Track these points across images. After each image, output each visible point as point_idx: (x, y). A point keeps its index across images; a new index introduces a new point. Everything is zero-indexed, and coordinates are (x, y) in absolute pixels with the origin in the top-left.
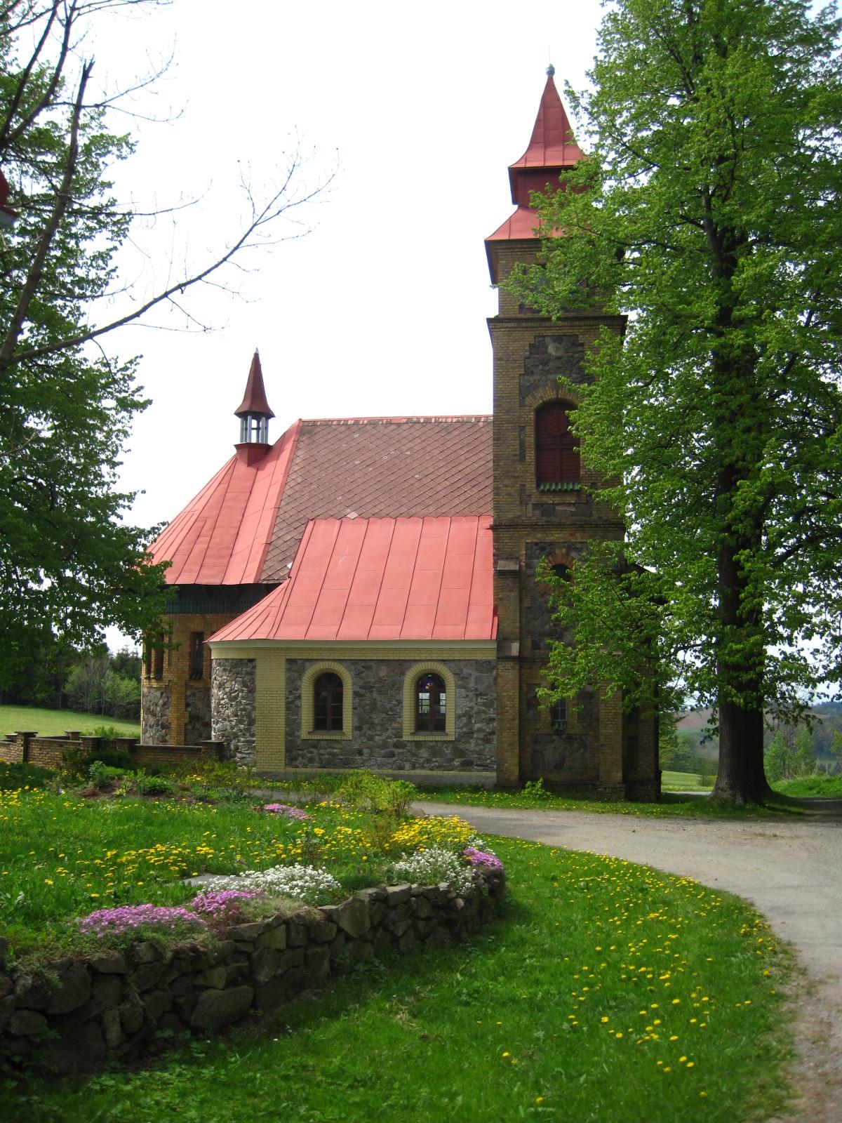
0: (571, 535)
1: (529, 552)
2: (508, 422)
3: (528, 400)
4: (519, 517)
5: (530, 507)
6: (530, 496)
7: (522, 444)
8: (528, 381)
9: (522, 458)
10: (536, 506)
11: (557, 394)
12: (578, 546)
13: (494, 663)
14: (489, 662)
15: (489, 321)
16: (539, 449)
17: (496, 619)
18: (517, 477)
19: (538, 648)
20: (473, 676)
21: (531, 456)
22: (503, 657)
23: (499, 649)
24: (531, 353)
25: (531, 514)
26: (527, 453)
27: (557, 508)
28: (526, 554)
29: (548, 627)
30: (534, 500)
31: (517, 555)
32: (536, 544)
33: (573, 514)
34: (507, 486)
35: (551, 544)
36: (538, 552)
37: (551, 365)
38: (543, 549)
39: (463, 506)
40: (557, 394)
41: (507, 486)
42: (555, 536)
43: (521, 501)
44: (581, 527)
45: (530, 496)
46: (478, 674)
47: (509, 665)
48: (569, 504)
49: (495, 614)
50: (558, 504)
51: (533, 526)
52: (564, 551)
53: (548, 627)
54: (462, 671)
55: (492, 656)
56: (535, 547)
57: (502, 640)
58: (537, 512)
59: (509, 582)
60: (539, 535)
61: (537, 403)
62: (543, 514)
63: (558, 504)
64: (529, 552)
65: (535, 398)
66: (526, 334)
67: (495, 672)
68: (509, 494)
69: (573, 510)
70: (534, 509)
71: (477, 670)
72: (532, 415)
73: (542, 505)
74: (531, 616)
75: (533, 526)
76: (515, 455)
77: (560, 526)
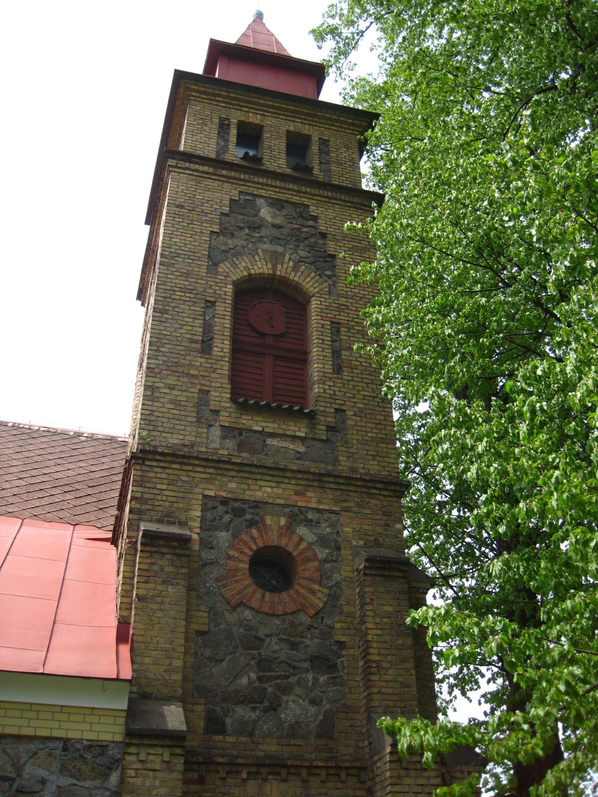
0: (297, 493)
1: (209, 515)
2: (183, 290)
3: (223, 267)
4: (193, 445)
5: (216, 432)
6: (216, 412)
7: (208, 328)
8: (225, 244)
9: (206, 346)
10: (228, 431)
11: (274, 268)
12: (310, 516)
13: (113, 752)
14: (100, 748)
15: (180, 77)
16: (238, 349)
17: (125, 649)
18: (193, 376)
19: (222, 731)
20: (51, 788)
21: (222, 346)
22: (141, 732)
23: (131, 713)
24: (231, 211)
25: (214, 442)
26: (217, 343)
27: (269, 441)
28: (203, 519)
29: (244, 681)
30: (225, 419)
31: (183, 518)
32: (225, 502)
33: (300, 456)
34: (172, 388)
35: (257, 505)
36: (227, 518)
37: (264, 232)
38: (238, 513)
39: (47, 509)
40: (274, 268)
41: (172, 388)
42: (265, 491)
43: (199, 420)
44: (319, 480)
45: (216, 412)
46: (66, 781)
47: (156, 757)
48: (294, 438)
49: (122, 636)
50: (273, 435)
51: (219, 465)
52: (283, 521)
53: (244, 681)
54: (19, 769)
55: (110, 731)
56: (221, 509)
57: (141, 695)
58: (230, 444)
59: (165, 563)
60: (232, 485)
61: (239, 274)
62: (241, 447)
63: (273, 435)
64: (209, 515)
65: (235, 266)
66: (226, 186)
67: (114, 778)
68: (176, 403)
69: (302, 449)
70: (223, 438)
71: (64, 770)
72: (229, 289)
73: (241, 431)
74: (208, 652)
75: (219, 465)
76: (192, 341)
77: (277, 472)
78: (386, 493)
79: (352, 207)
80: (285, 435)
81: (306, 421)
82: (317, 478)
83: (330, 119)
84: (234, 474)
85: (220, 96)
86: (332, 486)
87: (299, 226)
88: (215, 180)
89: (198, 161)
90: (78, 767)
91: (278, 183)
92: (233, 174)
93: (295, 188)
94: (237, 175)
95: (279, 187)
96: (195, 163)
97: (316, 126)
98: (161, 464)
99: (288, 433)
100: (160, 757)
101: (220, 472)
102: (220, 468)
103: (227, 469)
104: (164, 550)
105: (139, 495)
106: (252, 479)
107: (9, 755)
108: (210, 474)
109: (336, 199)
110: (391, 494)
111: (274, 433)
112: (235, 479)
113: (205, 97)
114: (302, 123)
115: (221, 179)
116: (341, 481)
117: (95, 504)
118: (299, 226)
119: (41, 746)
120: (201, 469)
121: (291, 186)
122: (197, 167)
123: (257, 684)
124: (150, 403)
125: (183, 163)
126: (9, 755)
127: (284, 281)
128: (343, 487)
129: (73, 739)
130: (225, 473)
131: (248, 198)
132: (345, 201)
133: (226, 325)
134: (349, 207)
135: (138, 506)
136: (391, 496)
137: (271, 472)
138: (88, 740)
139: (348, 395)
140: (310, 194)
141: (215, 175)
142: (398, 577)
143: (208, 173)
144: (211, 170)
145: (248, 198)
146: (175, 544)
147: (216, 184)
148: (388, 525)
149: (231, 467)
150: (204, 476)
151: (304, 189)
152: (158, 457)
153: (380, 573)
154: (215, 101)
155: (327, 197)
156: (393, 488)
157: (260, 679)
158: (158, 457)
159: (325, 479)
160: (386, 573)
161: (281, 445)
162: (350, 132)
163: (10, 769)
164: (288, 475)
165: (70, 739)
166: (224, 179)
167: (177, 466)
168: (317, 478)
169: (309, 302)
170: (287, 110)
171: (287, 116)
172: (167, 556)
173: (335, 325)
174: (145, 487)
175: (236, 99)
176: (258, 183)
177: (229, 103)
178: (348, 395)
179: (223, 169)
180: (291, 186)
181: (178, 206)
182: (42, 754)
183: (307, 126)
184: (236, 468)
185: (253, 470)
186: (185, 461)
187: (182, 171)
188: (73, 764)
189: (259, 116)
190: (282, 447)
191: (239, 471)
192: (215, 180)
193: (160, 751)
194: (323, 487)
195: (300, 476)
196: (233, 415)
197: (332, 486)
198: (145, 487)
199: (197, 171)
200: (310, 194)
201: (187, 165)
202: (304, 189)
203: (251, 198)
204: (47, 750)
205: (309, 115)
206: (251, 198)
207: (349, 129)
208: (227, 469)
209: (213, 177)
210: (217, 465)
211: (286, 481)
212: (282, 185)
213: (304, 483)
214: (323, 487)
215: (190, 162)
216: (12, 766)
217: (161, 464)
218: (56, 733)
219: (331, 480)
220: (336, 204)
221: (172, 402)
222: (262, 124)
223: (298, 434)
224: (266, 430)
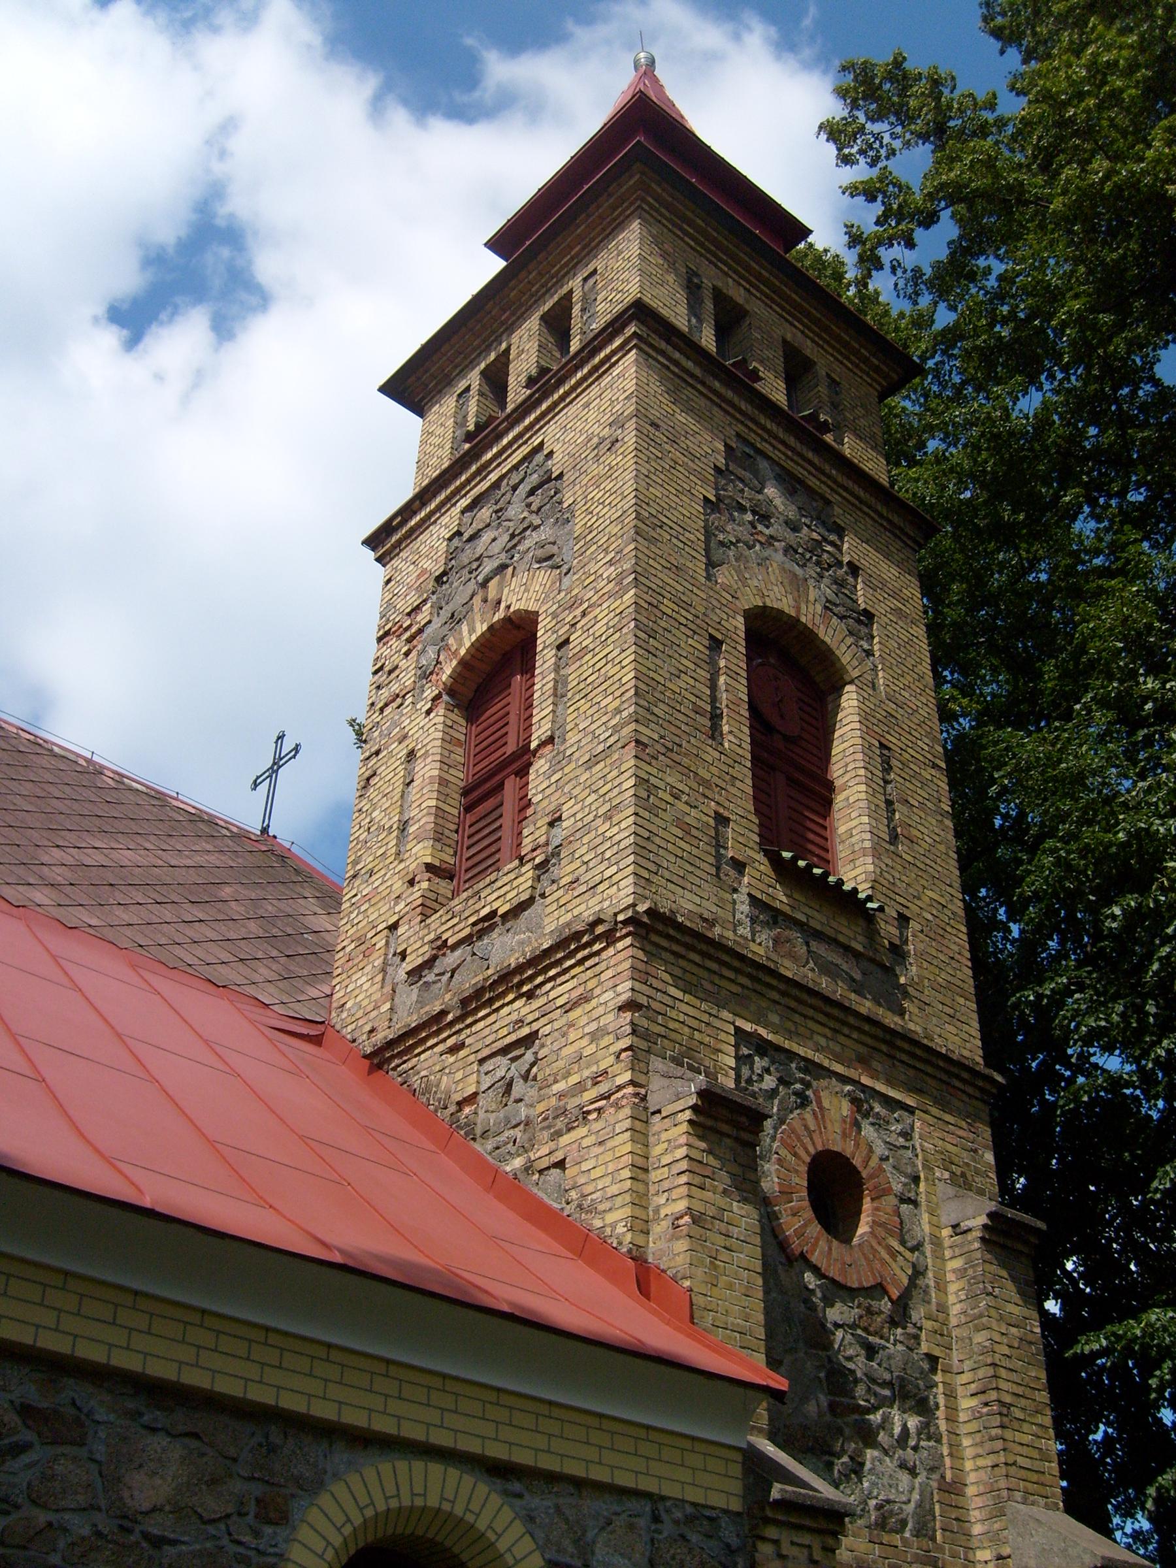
21: (736, 734)
78: (970, 1090)
79: (890, 531)
80: (835, 941)
81: (861, 922)
82: (888, 1037)
83: (846, 345)
84: (775, 996)
85: (690, 223)
86: (905, 1058)
87: (819, 538)
88: (701, 393)
89: (682, 345)
90: (678, 1557)
91: (792, 441)
92: (730, 394)
93: (816, 460)
94: (736, 400)
95: (793, 450)
96: (676, 347)
97: (822, 348)
98: (675, 948)
99: (841, 938)
100: (805, 1551)
101: (758, 987)
102: (758, 980)
103: (769, 986)
104: (725, 1128)
105: (643, 1000)
106: (801, 1015)
107: (567, 1521)
108: (742, 986)
109: (870, 507)
110: (978, 1094)
111: (822, 933)
112: (778, 1007)
113: (667, 214)
114: (803, 332)
115: (711, 395)
116: (919, 1052)
117: (13, 868)
118: (819, 538)
119: (618, 1509)
120: (732, 975)
121: (810, 455)
122: (677, 355)
123: (828, 1418)
124: (646, 815)
125: (657, 338)
126: (567, 1521)
127: (807, 637)
128: (918, 1065)
129: (670, 1498)
130: (764, 990)
131: (747, 450)
132: (881, 515)
133: (741, 695)
134: (885, 528)
135: (645, 1023)
136: (977, 1098)
137: (828, 1009)
138: (694, 1504)
139: (911, 890)
140: (835, 482)
141: (703, 383)
142: (1021, 1252)
143: (692, 375)
144: (698, 372)
145: (747, 450)
146: (743, 1119)
147: (703, 402)
148: (975, 1151)
149: (774, 982)
150: (735, 989)
151: (827, 468)
152: (671, 932)
153: (1002, 1240)
154: (681, 229)
155: (858, 498)
156: (981, 1084)
157: (832, 1407)
158: (671, 932)
159: (899, 1043)
160: (1009, 1243)
161: (830, 959)
162: (869, 381)
163: (571, 1549)
164: (851, 1020)
165: (663, 1498)
166: (715, 398)
167: (696, 958)
168: (888, 1037)
169: (837, 689)
170: (788, 299)
171: (783, 309)
172: (728, 1141)
173: (885, 752)
174: (651, 986)
175: (714, 241)
176: (764, 428)
177: (702, 245)
178: (911, 890)
179: (716, 377)
180: (810, 455)
181: (653, 424)
182: (619, 1522)
183: (809, 343)
184: (782, 986)
185: (805, 996)
186: (712, 951)
187: (654, 354)
188: (672, 1551)
189: (742, 291)
190: (832, 963)
191: (784, 994)
192: (701, 393)
193: (806, 1539)
194: (893, 1057)
195: (867, 1027)
196: (767, 880)
197: (905, 1058)
198: (651, 986)
199: (677, 363)
200: (835, 482)
201: (663, 345)
202: (827, 468)
203: (752, 453)
204: (624, 1516)
205: (817, 322)
206: (752, 453)
207: (868, 375)
208: (769, 986)
209: (699, 386)
210: (755, 973)
211: (846, 1031)
212: (798, 446)
213: (869, 1041)
214: (893, 1057)
215: (668, 342)
216: (576, 1542)
217: (675, 948)
218: (647, 1484)
219: (906, 1046)
220: (869, 516)
221: (679, 823)
222: (747, 307)
223: (854, 944)
224: (813, 923)
